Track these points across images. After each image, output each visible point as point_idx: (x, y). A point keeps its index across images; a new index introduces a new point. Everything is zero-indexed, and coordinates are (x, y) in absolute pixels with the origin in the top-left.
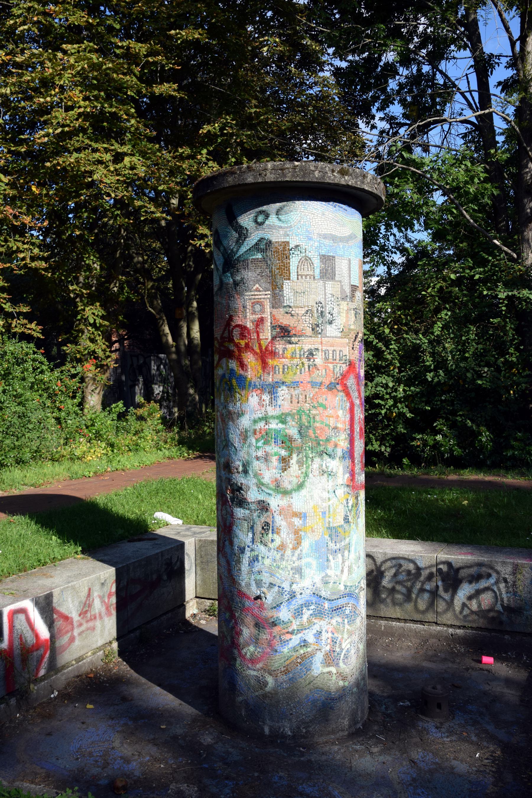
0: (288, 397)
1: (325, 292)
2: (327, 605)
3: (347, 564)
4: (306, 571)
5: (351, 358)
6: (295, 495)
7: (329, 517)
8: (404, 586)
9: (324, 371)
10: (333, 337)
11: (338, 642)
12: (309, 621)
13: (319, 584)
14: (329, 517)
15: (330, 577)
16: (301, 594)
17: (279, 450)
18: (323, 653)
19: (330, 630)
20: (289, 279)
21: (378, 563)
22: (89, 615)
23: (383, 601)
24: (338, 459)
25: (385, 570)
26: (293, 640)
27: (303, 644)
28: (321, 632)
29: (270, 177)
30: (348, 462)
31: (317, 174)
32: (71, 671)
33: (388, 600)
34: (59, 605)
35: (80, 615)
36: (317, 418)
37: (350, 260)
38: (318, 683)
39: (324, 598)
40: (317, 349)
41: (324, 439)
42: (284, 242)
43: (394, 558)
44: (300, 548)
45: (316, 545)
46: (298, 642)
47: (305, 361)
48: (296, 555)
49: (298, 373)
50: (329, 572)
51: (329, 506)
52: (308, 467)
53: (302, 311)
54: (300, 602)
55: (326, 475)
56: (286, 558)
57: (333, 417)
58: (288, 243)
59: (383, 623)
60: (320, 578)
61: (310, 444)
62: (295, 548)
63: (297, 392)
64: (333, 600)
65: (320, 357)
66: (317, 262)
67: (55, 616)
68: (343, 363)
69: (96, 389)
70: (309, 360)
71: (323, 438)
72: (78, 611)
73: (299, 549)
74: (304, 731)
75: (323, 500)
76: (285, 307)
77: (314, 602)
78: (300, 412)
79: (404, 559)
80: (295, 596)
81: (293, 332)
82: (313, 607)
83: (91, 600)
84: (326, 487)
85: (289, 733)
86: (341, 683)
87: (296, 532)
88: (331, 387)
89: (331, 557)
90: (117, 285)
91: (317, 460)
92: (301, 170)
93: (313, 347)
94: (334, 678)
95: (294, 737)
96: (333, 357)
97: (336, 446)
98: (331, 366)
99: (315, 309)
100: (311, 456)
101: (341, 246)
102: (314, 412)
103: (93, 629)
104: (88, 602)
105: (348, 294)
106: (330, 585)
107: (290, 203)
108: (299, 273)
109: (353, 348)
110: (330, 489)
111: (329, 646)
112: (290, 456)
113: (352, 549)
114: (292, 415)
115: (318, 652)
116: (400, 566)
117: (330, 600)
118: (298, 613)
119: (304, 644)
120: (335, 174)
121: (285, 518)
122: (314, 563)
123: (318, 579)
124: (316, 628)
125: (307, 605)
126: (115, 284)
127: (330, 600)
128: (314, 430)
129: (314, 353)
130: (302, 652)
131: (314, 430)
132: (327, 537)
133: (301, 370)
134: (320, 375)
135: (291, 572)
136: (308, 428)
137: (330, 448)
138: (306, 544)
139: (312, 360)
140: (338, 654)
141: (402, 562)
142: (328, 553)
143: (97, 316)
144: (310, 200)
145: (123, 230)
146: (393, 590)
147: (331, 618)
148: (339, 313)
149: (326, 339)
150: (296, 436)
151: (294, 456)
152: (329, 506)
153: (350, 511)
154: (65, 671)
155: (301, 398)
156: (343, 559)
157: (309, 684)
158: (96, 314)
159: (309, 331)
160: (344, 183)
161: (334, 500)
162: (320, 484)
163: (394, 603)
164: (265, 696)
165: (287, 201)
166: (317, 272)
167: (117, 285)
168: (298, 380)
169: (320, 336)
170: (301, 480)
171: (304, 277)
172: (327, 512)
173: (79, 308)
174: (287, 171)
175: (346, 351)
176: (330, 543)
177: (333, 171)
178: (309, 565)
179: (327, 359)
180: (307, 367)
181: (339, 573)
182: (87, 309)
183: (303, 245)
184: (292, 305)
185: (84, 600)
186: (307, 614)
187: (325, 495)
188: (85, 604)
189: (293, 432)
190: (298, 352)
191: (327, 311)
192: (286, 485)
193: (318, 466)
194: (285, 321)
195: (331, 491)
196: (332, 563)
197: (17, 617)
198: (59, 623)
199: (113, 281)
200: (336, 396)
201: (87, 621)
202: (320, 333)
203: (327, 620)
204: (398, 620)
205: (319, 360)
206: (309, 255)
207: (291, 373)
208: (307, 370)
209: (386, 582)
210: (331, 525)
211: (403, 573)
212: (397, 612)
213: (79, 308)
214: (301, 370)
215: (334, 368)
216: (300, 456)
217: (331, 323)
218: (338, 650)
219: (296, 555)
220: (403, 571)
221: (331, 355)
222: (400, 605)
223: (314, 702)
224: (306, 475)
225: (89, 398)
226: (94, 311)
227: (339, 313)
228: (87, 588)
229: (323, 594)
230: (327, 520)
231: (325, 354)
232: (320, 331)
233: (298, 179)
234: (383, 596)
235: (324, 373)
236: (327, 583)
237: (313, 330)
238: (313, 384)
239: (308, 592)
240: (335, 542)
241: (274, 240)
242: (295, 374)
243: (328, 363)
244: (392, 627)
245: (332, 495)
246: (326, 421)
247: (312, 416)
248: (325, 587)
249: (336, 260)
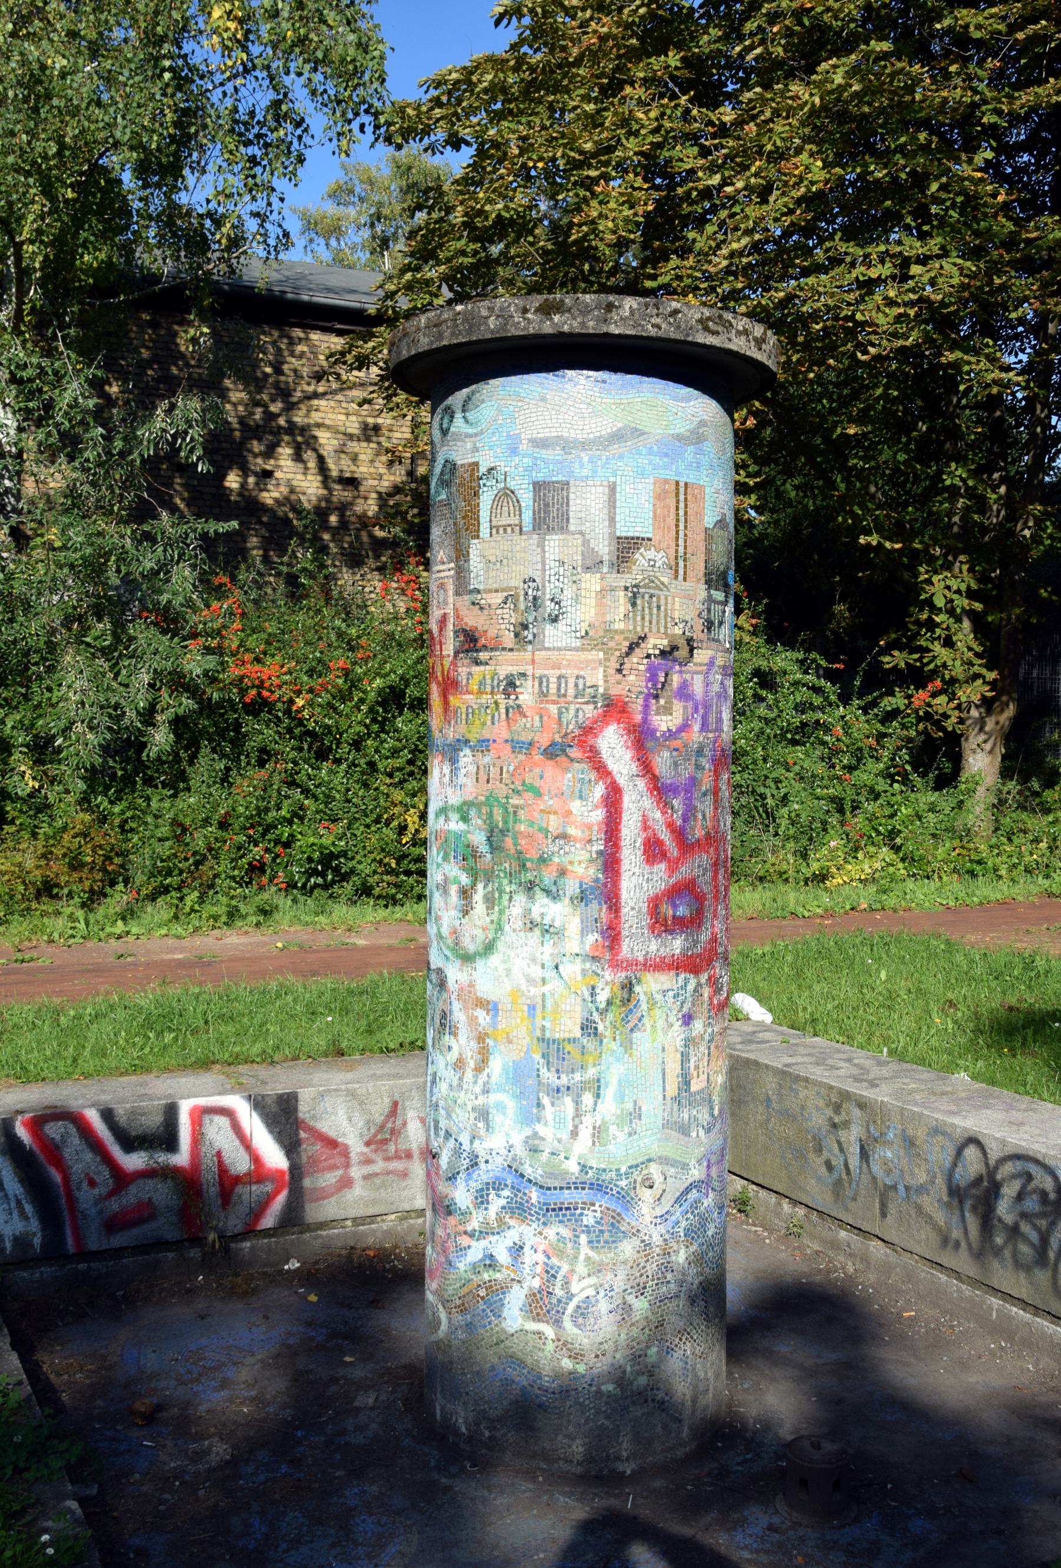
0: (472, 769)
1: (543, 557)
2: (534, 1195)
3: (588, 1120)
4: (496, 1118)
5: (614, 691)
6: (480, 963)
7: (544, 1018)
8: (1035, 1227)
9: (537, 718)
10: (559, 649)
11: (559, 1277)
12: (500, 1220)
13: (520, 1151)
14: (544, 1018)
15: (543, 1139)
16: (487, 1162)
17: (460, 872)
18: (525, 1291)
19: (541, 1248)
20: (478, 537)
21: (992, 1163)
22: (392, 1148)
23: (997, 1252)
24: (567, 900)
25: (1003, 1180)
26: (472, 1250)
27: (488, 1262)
28: (522, 1248)
29: (425, 343)
30: (598, 910)
31: (492, 323)
32: (338, 1235)
33: (1007, 1253)
34: (314, 1117)
35: (368, 1144)
36: (522, 814)
37: (613, 489)
38: (515, 1346)
39: (530, 1181)
40: (524, 675)
41: (536, 856)
42: (470, 465)
43: (1018, 1157)
44: (487, 1071)
45: (515, 1070)
46: (480, 1256)
47: (500, 697)
48: (480, 1082)
49: (489, 723)
50: (540, 1129)
51: (544, 995)
52: (501, 912)
53: (497, 599)
54: (485, 1178)
55: (537, 931)
56: (465, 1087)
57: (555, 813)
58: (477, 464)
59: (995, 1302)
60: (522, 1137)
61: (507, 865)
62: (478, 1070)
63: (487, 759)
64: (549, 1189)
65: (530, 690)
66: (526, 497)
67: (303, 1135)
68: (587, 703)
69: (985, 742)
70: (508, 696)
71: (533, 854)
72: (361, 1135)
73: (485, 1073)
74: (487, 1434)
75: (530, 981)
76: (471, 592)
77: (509, 1182)
78: (491, 800)
79: (1037, 1162)
80: (476, 1164)
81: (483, 641)
82: (506, 1193)
83: (399, 1122)
84: (538, 954)
85: (463, 1430)
86: (567, 1364)
87: (481, 1038)
88: (554, 752)
89: (546, 1101)
90: (1031, 524)
91: (520, 899)
92: (466, 320)
93: (514, 670)
94: (550, 1347)
95: (470, 1439)
96: (559, 689)
97: (563, 872)
98: (553, 709)
99: (522, 593)
100: (508, 889)
101: (586, 459)
102: (515, 801)
103: (405, 1175)
104: (389, 1125)
105: (606, 558)
106: (544, 1156)
107: (481, 386)
108: (494, 523)
109: (619, 671)
110: (546, 958)
111: (537, 1279)
112: (473, 886)
113: (609, 1093)
114: (478, 806)
115: (516, 1287)
116: (1029, 1177)
117: (541, 1187)
118: (481, 1199)
119: (490, 1262)
120: (529, 316)
121: (465, 1008)
122: (511, 1104)
123: (517, 1139)
124: (512, 1236)
125: (497, 1185)
126: (1026, 523)
127: (541, 1187)
128: (515, 838)
129: (518, 683)
130: (486, 1276)
131: (515, 838)
132: (537, 1057)
133: (493, 717)
134: (529, 727)
135: (473, 1115)
136: (504, 832)
137: (548, 877)
138: (496, 1065)
139: (513, 697)
140: (559, 1301)
141: (1033, 1169)
142: (539, 1091)
143: (958, 592)
144: (528, 372)
145: (1039, 407)
146: (1014, 1231)
147: (545, 1224)
148: (577, 599)
149: (543, 653)
150: (484, 848)
151: (480, 886)
152: (544, 995)
153: (603, 1013)
154: (324, 1233)
155: (494, 772)
156: (577, 1110)
157: (497, 1344)
158: (955, 588)
159: (508, 640)
160: (550, 331)
161: (554, 985)
162: (525, 949)
163: (1018, 1265)
164: (437, 1343)
165: (477, 382)
166: (527, 516)
167: (1031, 524)
168: (487, 737)
169: (530, 647)
170: (490, 937)
171: (501, 530)
172: (539, 1007)
173: (922, 578)
174: (444, 327)
175: (597, 677)
176: (544, 1071)
177: (525, 311)
178: (501, 1107)
179: (543, 695)
180: (503, 711)
181: (565, 1135)
182: (935, 579)
183: (502, 466)
184: (481, 587)
185: (379, 1119)
186: (496, 1204)
187: (536, 972)
188: (382, 1127)
189: (479, 839)
190: (489, 681)
191: (548, 596)
192: (470, 946)
193: (520, 910)
194: (473, 620)
195: (550, 964)
196: (549, 1112)
197: (211, 1121)
198: (310, 1149)
199: (1021, 517)
200: (566, 770)
201: (387, 1159)
202: (530, 642)
203: (534, 1225)
204: (1023, 1304)
205: (526, 696)
206: (512, 484)
207: (477, 722)
208: (503, 716)
209: (1004, 1208)
210: (548, 1035)
211: (1034, 1197)
212: (1018, 1284)
213: (922, 578)
214: (493, 717)
215: (560, 713)
216: (489, 888)
217: (555, 620)
218: (559, 1292)
219: (480, 1082)
220: (1034, 1191)
221: (553, 687)
222: (1028, 1269)
223: (507, 1382)
224: (500, 928)
225: (971, 760)
226: (948, 583)
227: (577, 599)
228: (387, 1102)
229: (528, 1171)
230: (539, 1022)
231: (541, 684)
232: (530, 637)
233: (445, 343)
234: (999, 1240)
235: (537, 724)
236: (536, 1151)
237: (517, 635)
238: (516, 746)
239: (499, 1160)
240: (558, 1071)
241: (459, 463)
242: (484, 724)
243: (547, 702)
244: (1011, 1318)
245: (550, 974)
246: (540, 820)
247: (511, 810)
248: (531, 1157)
249: (572, 490)
